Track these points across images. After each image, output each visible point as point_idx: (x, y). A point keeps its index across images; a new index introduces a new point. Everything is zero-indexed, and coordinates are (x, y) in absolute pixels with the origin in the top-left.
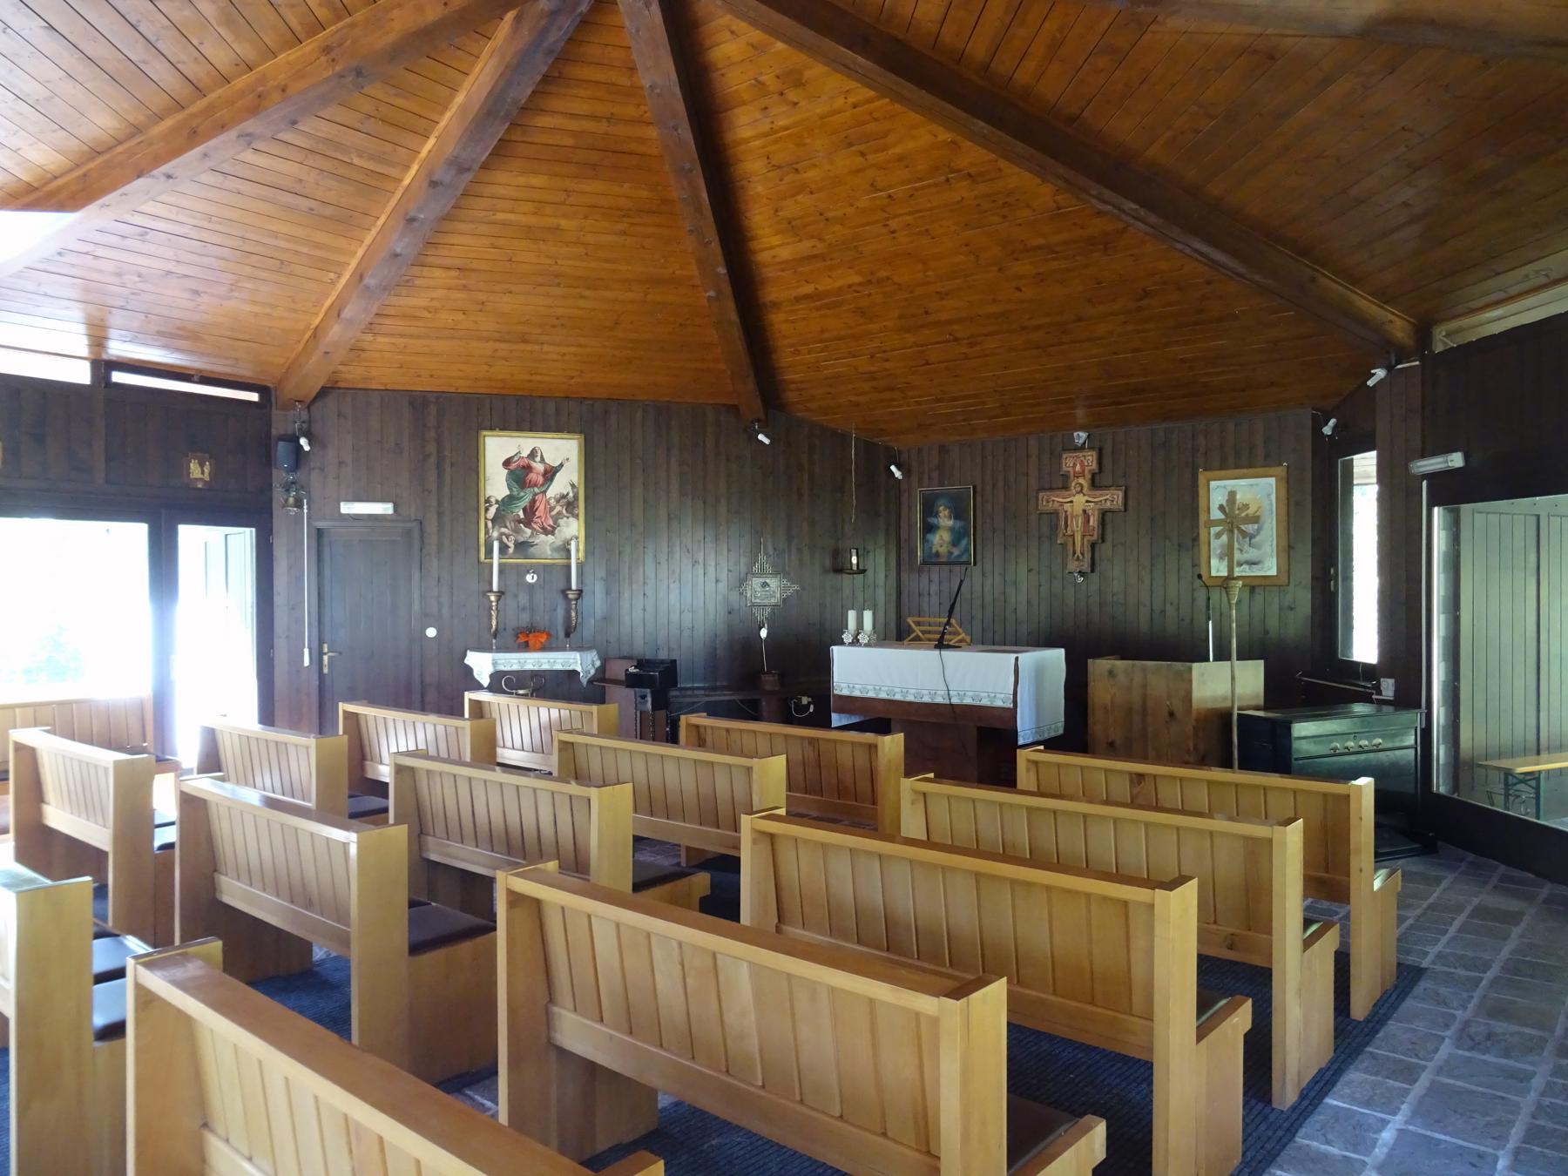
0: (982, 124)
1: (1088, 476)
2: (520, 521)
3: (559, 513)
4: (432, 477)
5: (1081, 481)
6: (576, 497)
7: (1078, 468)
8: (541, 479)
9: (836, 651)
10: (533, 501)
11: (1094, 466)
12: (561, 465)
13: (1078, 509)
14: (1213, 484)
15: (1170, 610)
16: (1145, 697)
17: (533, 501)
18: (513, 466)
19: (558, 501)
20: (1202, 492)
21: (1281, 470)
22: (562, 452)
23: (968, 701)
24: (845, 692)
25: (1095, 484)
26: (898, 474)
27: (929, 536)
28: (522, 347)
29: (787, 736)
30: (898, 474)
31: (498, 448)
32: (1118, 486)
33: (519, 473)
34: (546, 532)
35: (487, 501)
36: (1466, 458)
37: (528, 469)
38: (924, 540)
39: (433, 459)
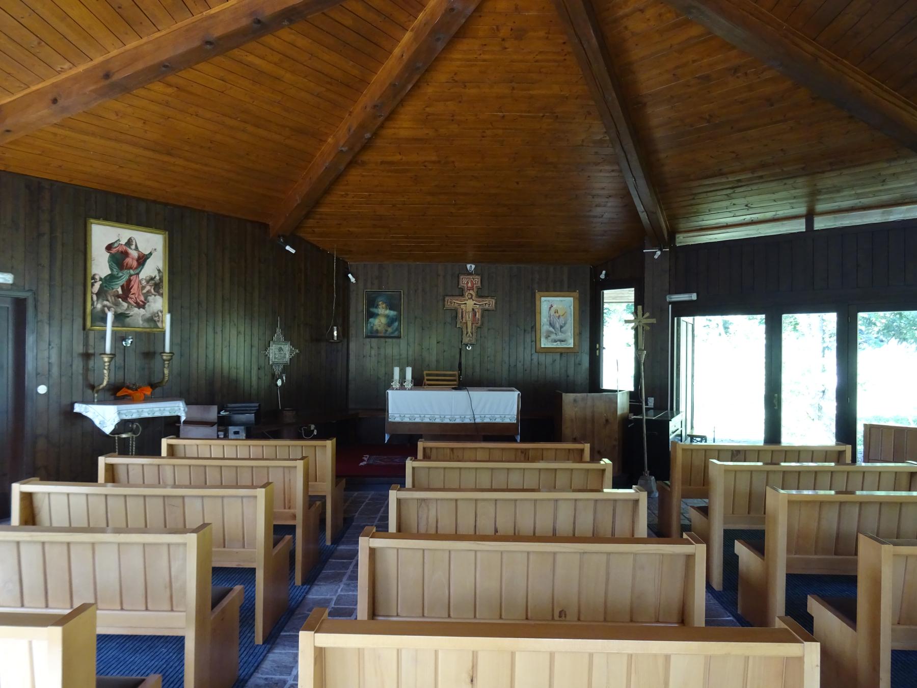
0: (614, 95)
1: (475, 290)
2: (118, 296)
3: (149, 292)
4: (45, 253)
5: (471, 292)
6: (161, 280)
7: (470, 285)
8: (135, 264)
9: (390, 392)
10: (129, 281)
11: (479, 284)
12: (151, 254)
13: (470, 308)
14: (543, 299)
15: (519, 365)
16: (593, 412)
17: (129, 281)
18: (114, 251)
19: (148, 282)
20: (537, 303)
21: (576, 294)
22: (151, 242)
23: (487, 420)
24: (398, 420)
25: (480, 295)
26: (353, 280)
27: (371, 320)
28: (166, 158)
29: (503, 449)
30: (353, 280)
31: (103, 235)
32: (492, 297)
33: (118, 257)
34: (139, 306)
35: (93, 278)
36: (698, 296)
37: (126, 254)
38: (367, 323)
39: (46, 238)
